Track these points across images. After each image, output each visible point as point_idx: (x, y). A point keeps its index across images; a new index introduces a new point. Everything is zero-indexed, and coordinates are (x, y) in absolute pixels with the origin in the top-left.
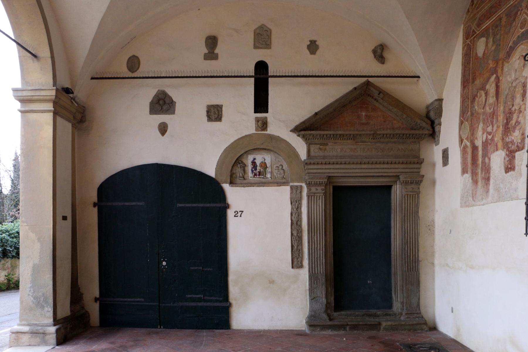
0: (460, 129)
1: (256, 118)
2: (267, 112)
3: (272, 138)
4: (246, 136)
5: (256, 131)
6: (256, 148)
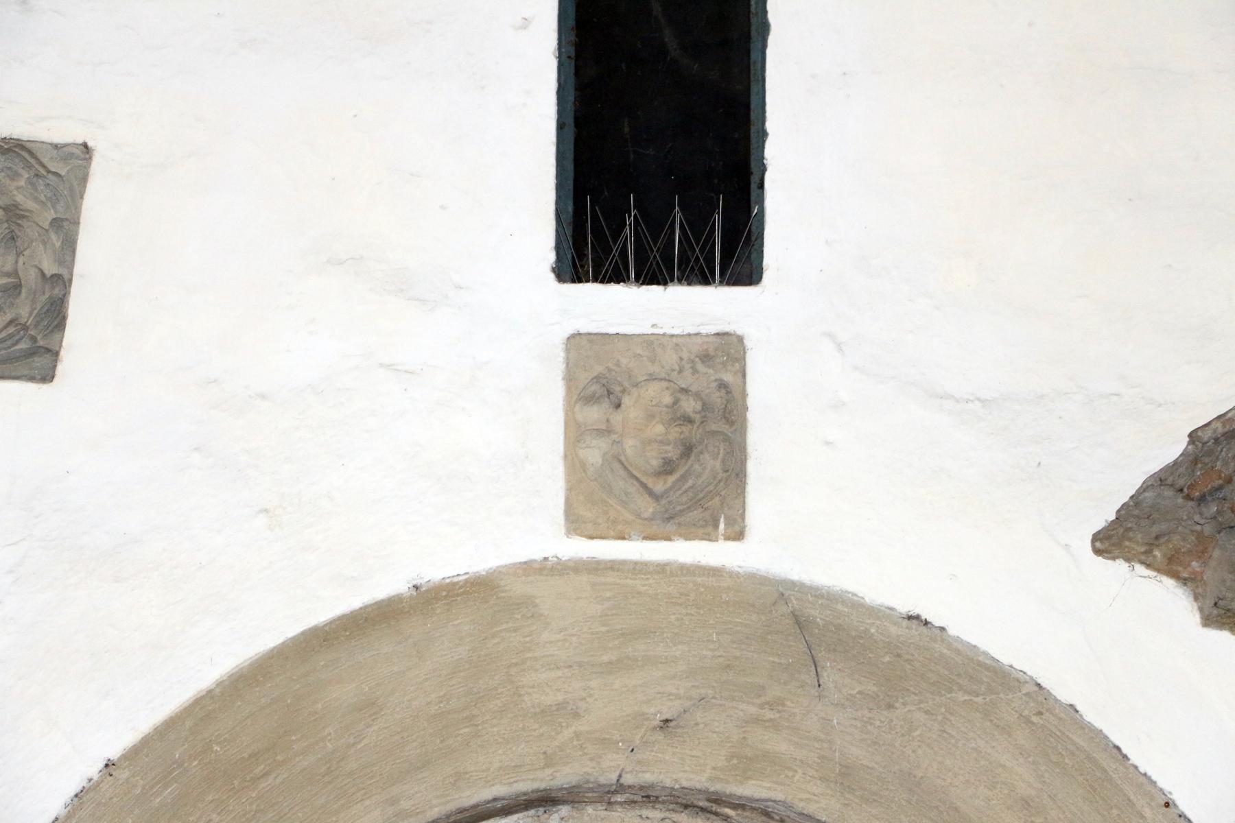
0: (51, 144)
1: (583, 347)
2: (731, 250)
3: (811, 632)
4: (430, 600)
5: (575, 524)
6: (564, 776)
